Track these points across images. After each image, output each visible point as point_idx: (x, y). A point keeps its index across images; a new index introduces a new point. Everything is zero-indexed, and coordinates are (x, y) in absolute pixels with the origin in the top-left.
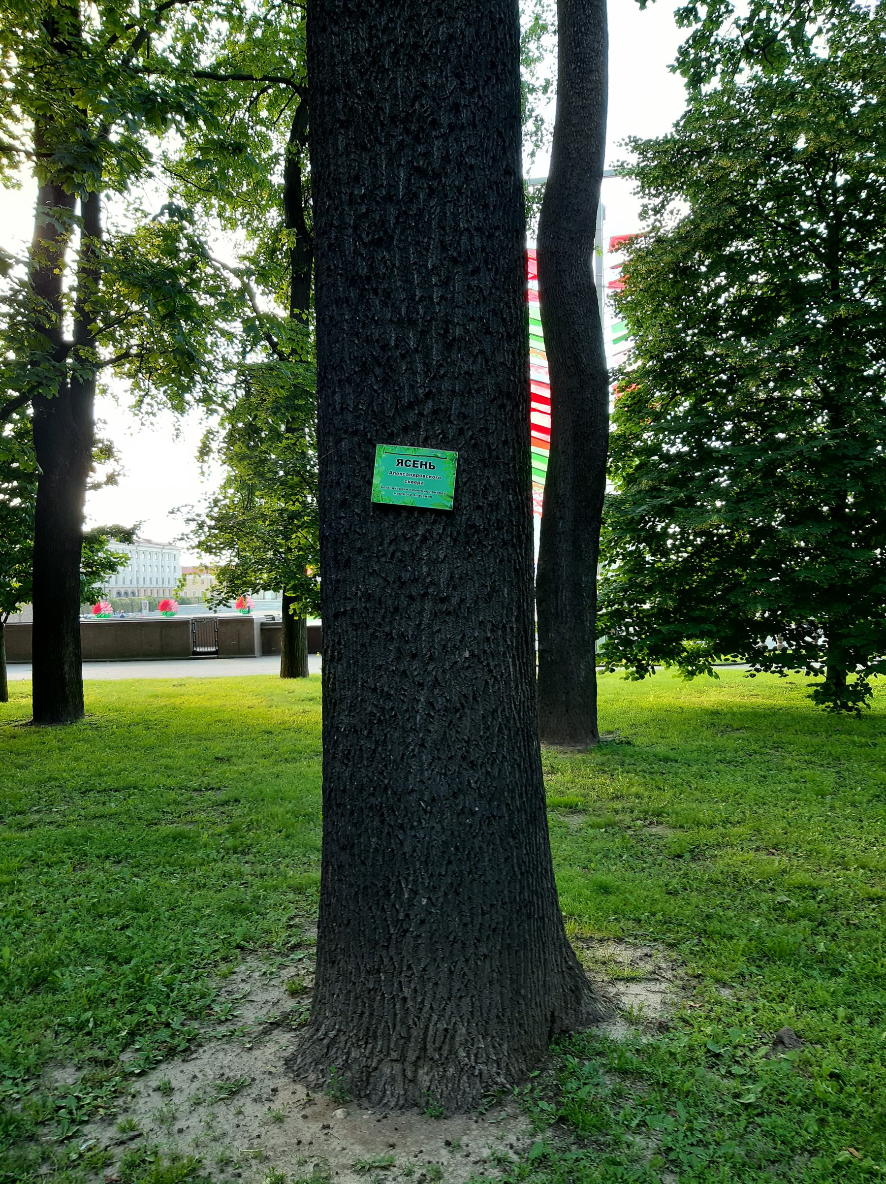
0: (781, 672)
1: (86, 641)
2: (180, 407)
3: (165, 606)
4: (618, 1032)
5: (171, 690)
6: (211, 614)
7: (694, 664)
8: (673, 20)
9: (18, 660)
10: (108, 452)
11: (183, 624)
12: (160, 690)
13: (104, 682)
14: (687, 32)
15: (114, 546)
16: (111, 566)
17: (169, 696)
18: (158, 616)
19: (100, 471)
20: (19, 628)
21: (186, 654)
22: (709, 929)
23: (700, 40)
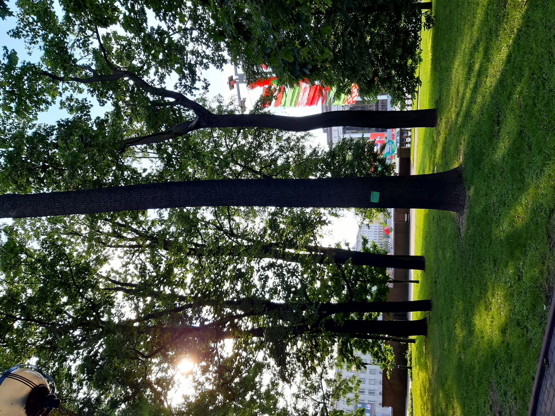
0: (420, 41)
1: (401, 253)
2: (172, 378)
3: (388, 231)
4: (110, 224)
5: (418, 231)
6: (392, 218)
7: (417, 60)
8: (208, 70)
9: (406, 316)
10: (338, 245)
11: (396, 225)
12: (418, 234)
13: (415, 250)
14: (211, 65)
15: (369, 246)
16: (375, 246)
17: (420, 231)
18: (392, 234)
19: (344, 247)
20: (395, 274)
22: (77, 359)
23: (213, 62)
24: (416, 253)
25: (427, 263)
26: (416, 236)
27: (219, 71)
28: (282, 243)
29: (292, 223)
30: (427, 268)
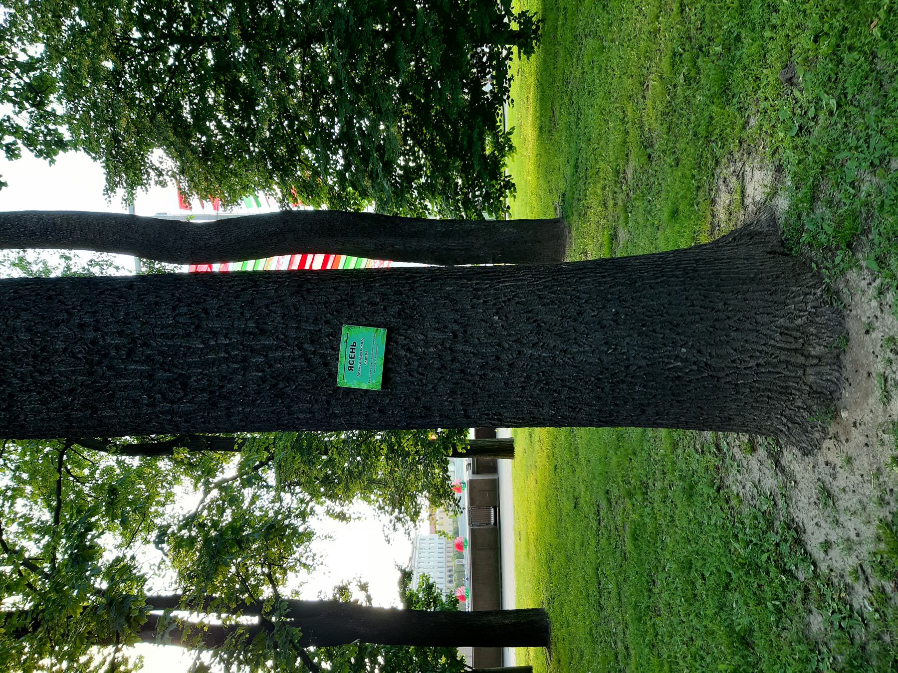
1: (486, 607)
3: (460, 547)
5: (523, 542)
6: (466, 512)
8: (15, 162)
10: (343, 590)
11: (473, 532)
12: (524, 551)
13: (517, 595)
14: (24, 151)
15: (414, 585)
17: (528, 543)
18: (467, 552)
19: (357, 596)
21: (496, 531)
23: (30, 141)
24: (519, 600)
25: (557, 632)
26: (517, 557)
27: (43, 162)
28: (296, 85)
29: (469, 209)
30: (560, 647)
